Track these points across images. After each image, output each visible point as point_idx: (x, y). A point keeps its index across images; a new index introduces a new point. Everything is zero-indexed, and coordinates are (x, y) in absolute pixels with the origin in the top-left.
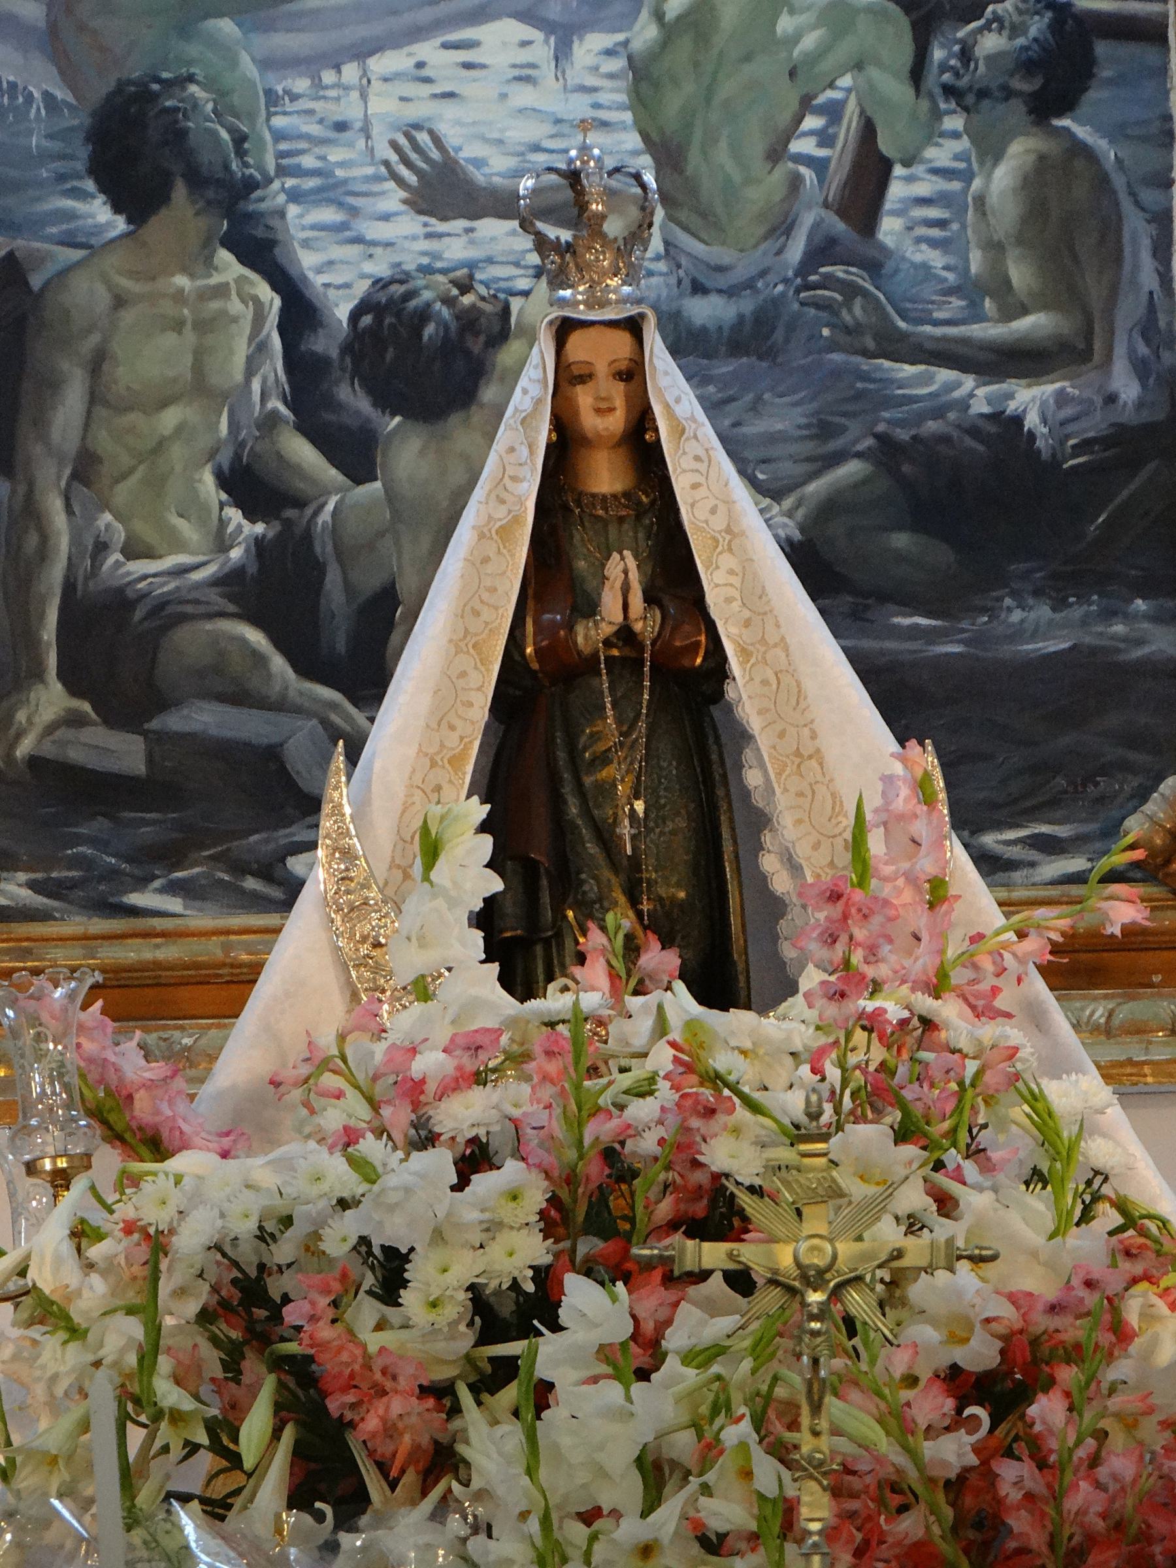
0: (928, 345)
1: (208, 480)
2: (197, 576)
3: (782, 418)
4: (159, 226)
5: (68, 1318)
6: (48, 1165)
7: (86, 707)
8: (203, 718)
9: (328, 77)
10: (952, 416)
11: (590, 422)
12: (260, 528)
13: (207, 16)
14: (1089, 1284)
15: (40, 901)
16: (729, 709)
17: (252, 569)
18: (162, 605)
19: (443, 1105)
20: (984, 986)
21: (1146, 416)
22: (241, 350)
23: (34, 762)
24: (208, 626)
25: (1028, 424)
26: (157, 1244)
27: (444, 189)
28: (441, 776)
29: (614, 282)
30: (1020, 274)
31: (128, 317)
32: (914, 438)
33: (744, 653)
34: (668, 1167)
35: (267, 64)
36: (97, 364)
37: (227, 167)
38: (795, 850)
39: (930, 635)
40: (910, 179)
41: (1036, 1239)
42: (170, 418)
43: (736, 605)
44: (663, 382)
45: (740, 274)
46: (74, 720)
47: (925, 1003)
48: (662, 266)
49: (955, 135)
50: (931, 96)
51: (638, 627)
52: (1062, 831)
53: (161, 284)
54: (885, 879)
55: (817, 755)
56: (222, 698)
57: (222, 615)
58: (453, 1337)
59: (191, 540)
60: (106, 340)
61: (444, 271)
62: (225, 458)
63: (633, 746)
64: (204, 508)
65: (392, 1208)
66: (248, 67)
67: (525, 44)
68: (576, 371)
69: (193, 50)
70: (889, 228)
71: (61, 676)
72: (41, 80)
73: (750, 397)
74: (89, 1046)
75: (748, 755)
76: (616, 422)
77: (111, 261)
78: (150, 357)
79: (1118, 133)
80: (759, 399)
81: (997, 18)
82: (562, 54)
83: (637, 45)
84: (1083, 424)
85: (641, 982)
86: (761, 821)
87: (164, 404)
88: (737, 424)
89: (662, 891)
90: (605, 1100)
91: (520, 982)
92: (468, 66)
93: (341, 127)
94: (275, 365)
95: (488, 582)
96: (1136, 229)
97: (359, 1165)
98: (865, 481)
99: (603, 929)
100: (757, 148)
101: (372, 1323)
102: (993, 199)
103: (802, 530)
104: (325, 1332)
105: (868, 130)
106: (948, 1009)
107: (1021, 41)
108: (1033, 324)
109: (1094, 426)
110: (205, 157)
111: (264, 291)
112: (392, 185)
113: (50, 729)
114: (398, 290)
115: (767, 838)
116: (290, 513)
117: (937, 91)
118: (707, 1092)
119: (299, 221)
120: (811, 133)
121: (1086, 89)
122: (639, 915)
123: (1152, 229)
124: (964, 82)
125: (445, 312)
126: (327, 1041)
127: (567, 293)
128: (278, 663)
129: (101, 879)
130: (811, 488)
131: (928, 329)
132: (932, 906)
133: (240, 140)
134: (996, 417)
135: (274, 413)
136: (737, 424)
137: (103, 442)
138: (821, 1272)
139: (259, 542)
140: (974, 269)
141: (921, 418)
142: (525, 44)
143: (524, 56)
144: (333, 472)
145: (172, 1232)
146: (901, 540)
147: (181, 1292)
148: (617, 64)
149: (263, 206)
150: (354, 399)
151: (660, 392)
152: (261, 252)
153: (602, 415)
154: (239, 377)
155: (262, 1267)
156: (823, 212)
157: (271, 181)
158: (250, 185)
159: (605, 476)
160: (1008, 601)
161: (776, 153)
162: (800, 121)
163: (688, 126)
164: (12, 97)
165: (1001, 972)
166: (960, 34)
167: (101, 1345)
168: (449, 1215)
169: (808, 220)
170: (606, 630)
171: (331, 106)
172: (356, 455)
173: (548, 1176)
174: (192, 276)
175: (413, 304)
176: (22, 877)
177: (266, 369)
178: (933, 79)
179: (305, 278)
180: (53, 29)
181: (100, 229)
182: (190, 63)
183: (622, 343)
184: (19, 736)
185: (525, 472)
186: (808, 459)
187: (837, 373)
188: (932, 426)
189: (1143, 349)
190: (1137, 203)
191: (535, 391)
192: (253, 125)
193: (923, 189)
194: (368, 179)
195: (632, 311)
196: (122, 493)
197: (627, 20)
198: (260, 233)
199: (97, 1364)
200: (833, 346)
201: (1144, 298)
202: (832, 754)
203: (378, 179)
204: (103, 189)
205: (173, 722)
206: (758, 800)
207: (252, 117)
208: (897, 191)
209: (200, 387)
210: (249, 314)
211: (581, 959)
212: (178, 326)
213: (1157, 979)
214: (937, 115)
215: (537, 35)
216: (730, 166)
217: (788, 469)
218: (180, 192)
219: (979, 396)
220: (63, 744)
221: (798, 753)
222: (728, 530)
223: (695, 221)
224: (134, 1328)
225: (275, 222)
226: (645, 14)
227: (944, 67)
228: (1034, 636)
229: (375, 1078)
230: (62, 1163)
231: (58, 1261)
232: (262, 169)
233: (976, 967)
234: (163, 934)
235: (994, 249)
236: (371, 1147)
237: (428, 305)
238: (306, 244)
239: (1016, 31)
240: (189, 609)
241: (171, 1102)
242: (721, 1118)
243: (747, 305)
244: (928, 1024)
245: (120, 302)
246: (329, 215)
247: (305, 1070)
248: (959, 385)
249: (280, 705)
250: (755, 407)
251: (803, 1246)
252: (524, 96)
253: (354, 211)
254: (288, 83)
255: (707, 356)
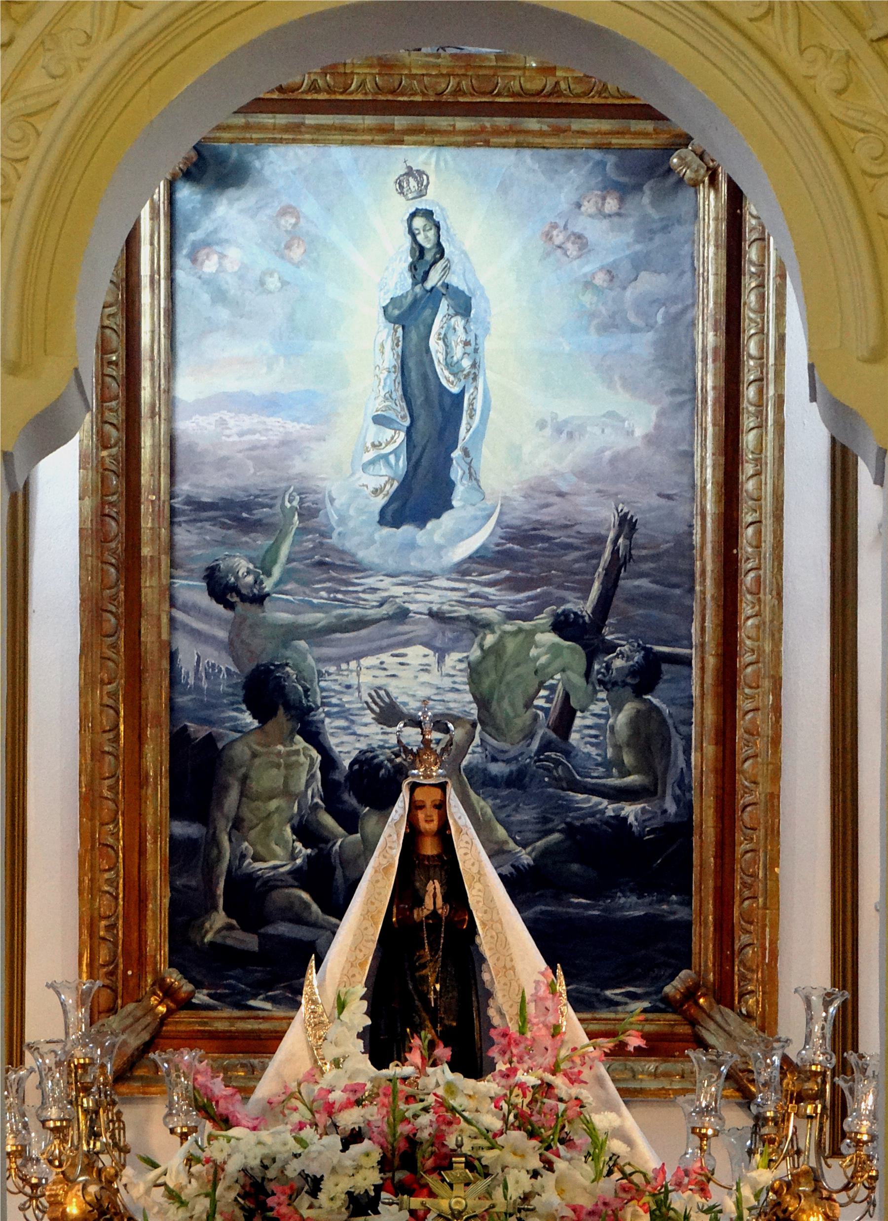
0: (589, 786)
1: (288, 830)
2: (282, 870)
3: (527, 814)
4: (270, 725)
5: (180, 1197)
6: (179, 1130)
7: (234, 922)
8: (283, 929)
9: (344, 666)
10: (598, 816)
11: (424, 826)
12: (309, 851)
13: (293, 640)
14: (605, 1204)
15: (212, 1002)
16: (477, 947)
17: (305, 868)
18: (269, 879)
19: (341, 1114)
20: (576, 1070)
21: (678, 820)
22: (304, 778)
23: (211, 943)
24: (286, 891)
25: (629, 821)
26: (218, 1169)
27: (389, 714)
28: (356, 970)
29: (434, 768)
30: (628, 759)
31: (257, 761)
32: (582, 825)
33: (484, 924)
34: (433, 1145)
35: (318, 660)
36: (244, 780)
37: (301, 702)
38: (502, 1010)
39: (586, 907)
40: (583, 718)
41: (587, 1183)
42: (273, 804)
43: (481, 904)
44: (454, 810)
45: (511, 754)
46: (229, 927)
47: (549, 1077)
48: (479, 750)
49: (603, 700)
50: (593, 684)
51: (440, 911)
52: (639, 990)
53: (271, 749)
54: (533, 1024)
55: (513, 968)
56: (291, 921)
57: (292, 886)
58: (340, 1213)
59: (279, 854)
60: (248, 770)
61: (389, 748)
62: (296, 821)
63: (436, 961)
64: (287, 842)
65: (313, 1159)
66: (311, 660)
67: (425, 656)
68: (418, 804)
69: (288, 653)
70: (574, 737)
71: (224, 909)
72: (225, 663)
73: (513, 805)
74: (201, 1079)
75: (484, 966)
76: (433, 826)
77: (252, 738)
78: (267, 778)
79: (671, 702)
80: (518, 806)
81: (621, 653)
82: (441, 661)
83: (472, 658)
84: (652, 822)
85: (435, 1060)
86: (489, 994)
87: (271, 798)
88: (508, 816)
89: (447, 1022)
90: (408, 1114)
91: (379, 1060)
92: (402, 664)
93: (348, 687)
94: (318, 784)
95: (378, 890)
96: (677, 743)
97: (300, 1141)
98: (562, 841)
99: (420, 1038)
100: (520, 702)
101: (307, 1206)
102: (617, 728)
103: (534, 860)
104: (284, 1210)
105: (567, 697)
106: (559, 1081)
107: (631, 663)
108: (633, 779)
109: (656, 823)
110: (292, 697)
111: (314, 753)
112: (368, 712)
113: (219, 931)
114: (370, 755)
115: (491, 1002)
116: (321, 845)
117: (596, 682)
118: (449, 1116)
119: (330, 725)
120: (542, 697)
121: (657, 684)
122: (436, 1031)
123: (683, 742)
124: (607, 679)
125: (389, 765)
126: (293, 1086)
127: (415, 772)
128: (315, 907)
129: (238, 994)
130: (539, 844)
131: (589, 780)
132: (553, 1036)
133: (306, 690)
134: (617, 817)
135: (317, 803)
136: (508, 816)
137: (246, 813)
138: (460, 1212)
139: (309, 857)
140: (609, 756)
141: (584, 817)
142: (425, 656)
143: (425, 661)
144: (340, 829)
145: (225, 1163)
146: (575, 867)
147: (229, 1188)
148: (464, 665)
149: (315, 718)
150: (350, 799)
151: (452, 815)
152: (314, 737)
153: (428, 824)
154: (303, 788)
155: (263, 1178)
156: (547, 730)
157: (318, 708)
158: (310, 709)
159: (429, 848)
160: (619, 894)
161: (528, 705)
162: (538, 691)
163: (492, 694)
164: (213, 670)
165: (583, 1064)
166: (606, 659)
167: (193, 1209)
168: (339, 1161)
169: (540, 732)
170: (426, 912)
171: (344, 678)
172: (350, 822)
173: (382, 1147)
174: (285, 746)
175: (376, 761)
176: (205, 991)
177: (314, 785)
178: (594, 677)
179: (331, 749)
180: (231, 643)
181: (247, 725)
182: (287, 658)
183: (437, 794)
184: (207, 932)
185: (395, 845)
186: (538, 832)
187: (551, 797)
188: (590, 820)
189: (678, 792)
190: (677, 731)
191: (401, 811)
192: (312, 685)
193: (589, 722)
194: (359, 709)
195: (442, 780)
196: (253, 834)
197: (468, 648)
198: (314, 729)
199: (191, 1217)
200: (549, 785)
201: (679, 771)
202: (519, 967)
203: (363, 709)
204: (248, 709)
205: (271, 930)
206: (488, 986)
207: (312, 681)
208: (578, 722)
209: (286, 792)
210: (308, 762)
211: (411, 1049)
212: (278, 766)
213: (677, 1054)
214: (595, 692)
215: (431, 652)
216: (509, 710)
217: (529, 835)
218: (281, 711)
219: (610, 808)
220: (225, 937)
221: (505, 967)
222: (479, 872)
223: (493, 732)
224: (206, 1202)
225: (320, 725)
226: (475, 646)
227: (599, 672)
228: (630, 909)
229: (313, 1101)
230: (185, 1130)
231: (178, 1173)
232: (315, 702)
233: (573, 1061)
234: (263, 1018)
235: (618, 748)
236: (308, 1133)
237: (382, 762)
238: (332, 734)
239: (629, 658)
240: (279, 883)
241: (233, 1105)
242: (455, 1126)
243: (514, 767)
244: (550, 1086)
245: (255, 755)
246: (342, 723)
247: (283, 1097)
248: (601, 804)
249: (315, 925)
250: (516, 810)
251: (453, 1201)
252: (424, 677)
253: (353, 722)
254: (327, 668)
255: (496, 787)
